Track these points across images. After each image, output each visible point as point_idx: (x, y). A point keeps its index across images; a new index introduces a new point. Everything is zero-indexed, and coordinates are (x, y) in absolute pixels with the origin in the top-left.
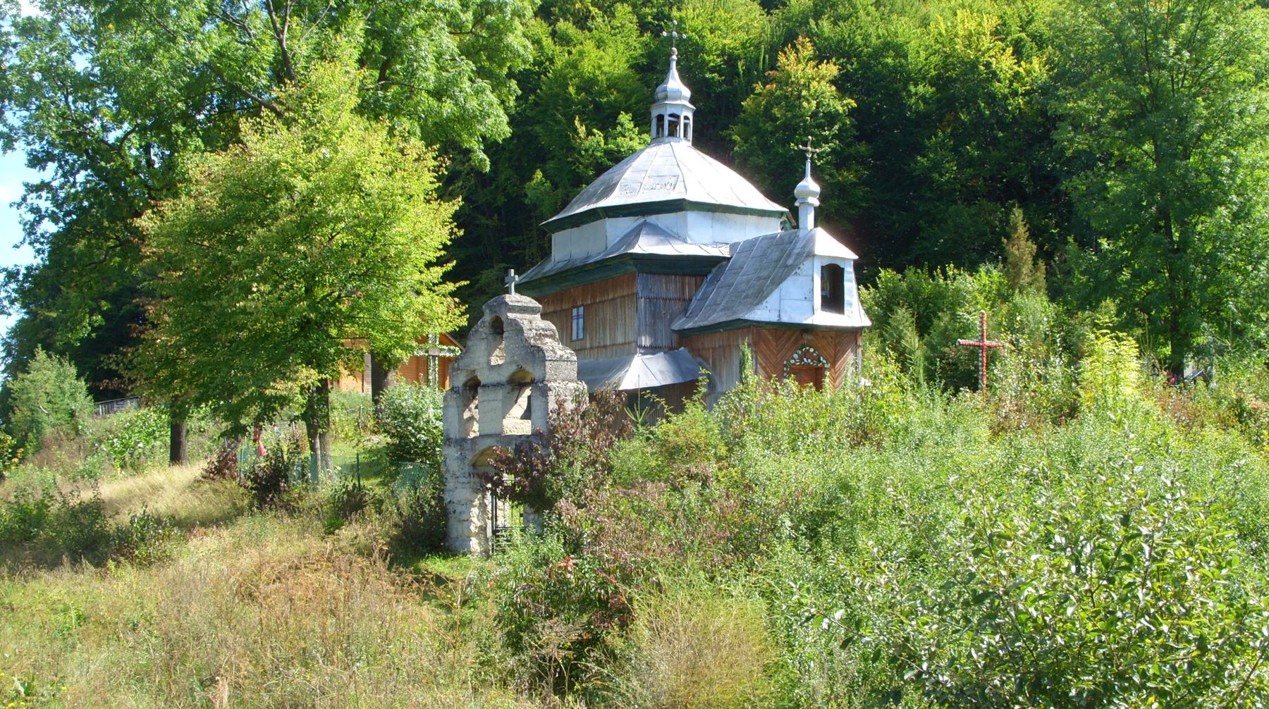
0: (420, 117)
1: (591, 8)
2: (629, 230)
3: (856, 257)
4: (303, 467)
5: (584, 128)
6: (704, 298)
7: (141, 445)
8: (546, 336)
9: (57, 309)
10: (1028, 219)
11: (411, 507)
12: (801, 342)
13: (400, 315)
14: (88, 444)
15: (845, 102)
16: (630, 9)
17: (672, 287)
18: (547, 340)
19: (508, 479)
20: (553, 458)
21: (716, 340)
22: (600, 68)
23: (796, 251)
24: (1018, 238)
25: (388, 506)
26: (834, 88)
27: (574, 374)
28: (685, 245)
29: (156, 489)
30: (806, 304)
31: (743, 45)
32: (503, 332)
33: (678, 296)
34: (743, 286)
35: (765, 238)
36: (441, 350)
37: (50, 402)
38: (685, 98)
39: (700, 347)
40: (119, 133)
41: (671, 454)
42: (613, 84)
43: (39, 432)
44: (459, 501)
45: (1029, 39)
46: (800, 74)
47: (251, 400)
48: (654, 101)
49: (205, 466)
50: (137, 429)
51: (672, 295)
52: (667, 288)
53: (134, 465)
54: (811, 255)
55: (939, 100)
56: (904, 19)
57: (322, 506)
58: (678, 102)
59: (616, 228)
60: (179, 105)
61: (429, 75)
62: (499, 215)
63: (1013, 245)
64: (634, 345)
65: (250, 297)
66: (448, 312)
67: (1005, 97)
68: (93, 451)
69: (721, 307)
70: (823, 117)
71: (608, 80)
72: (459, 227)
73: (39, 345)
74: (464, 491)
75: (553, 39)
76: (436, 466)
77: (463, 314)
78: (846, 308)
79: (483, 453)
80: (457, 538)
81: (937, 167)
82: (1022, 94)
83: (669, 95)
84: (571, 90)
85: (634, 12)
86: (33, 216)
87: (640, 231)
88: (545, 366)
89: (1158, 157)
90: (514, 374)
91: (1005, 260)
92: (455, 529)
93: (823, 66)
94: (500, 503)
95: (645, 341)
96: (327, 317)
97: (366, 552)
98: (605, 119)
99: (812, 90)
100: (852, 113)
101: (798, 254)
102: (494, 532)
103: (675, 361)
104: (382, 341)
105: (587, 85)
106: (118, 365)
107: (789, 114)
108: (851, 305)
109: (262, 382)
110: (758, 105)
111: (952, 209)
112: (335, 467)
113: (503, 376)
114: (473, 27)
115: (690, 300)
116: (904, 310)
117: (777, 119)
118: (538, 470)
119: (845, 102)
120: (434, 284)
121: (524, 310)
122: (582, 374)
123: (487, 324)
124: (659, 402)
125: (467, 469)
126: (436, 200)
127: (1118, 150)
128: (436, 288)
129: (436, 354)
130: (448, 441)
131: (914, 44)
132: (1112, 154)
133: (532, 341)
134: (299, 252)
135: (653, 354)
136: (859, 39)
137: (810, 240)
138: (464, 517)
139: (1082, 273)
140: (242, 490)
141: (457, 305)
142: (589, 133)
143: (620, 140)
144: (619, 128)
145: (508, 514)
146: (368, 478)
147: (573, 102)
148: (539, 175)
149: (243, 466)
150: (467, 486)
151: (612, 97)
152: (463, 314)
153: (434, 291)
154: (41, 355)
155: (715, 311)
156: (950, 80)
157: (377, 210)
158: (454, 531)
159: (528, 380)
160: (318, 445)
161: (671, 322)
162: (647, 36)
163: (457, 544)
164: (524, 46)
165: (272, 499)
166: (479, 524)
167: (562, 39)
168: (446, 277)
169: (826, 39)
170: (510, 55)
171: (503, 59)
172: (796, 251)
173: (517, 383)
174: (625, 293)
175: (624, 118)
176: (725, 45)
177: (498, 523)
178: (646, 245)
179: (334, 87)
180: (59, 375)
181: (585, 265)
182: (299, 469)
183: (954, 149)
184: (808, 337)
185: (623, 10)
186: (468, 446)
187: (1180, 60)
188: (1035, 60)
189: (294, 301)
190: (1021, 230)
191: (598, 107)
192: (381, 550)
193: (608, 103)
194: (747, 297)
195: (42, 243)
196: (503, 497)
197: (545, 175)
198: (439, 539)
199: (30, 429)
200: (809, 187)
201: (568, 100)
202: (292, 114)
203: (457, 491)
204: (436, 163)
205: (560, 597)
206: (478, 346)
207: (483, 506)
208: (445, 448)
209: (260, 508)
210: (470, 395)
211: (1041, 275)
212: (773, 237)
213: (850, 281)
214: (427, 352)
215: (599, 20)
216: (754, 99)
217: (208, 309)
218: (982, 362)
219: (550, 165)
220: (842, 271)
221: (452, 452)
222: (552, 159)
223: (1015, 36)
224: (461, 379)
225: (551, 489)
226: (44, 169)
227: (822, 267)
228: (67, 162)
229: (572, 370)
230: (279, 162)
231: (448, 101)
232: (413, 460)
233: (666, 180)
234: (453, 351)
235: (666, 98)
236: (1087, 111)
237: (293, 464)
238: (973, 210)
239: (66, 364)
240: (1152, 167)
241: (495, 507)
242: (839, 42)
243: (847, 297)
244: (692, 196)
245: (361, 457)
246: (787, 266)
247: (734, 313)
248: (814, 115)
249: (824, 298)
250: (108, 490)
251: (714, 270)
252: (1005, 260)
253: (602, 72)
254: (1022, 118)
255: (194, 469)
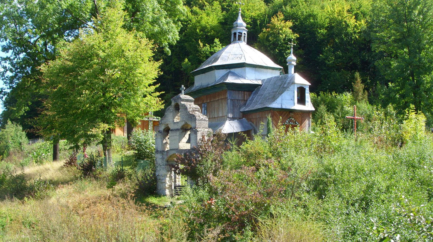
0: (146, 32)
1: (205, 3)
2: (224, 74)
3: (310, 84)
4: (101, 162)
5: (202, 44)
6: (252, 99)
7: (44, 154)
8: (196, 111)
9: (16, 107)
10: (360, 75)
11: (143, 178)
12: (289, 116)
13: (139, 103)
14: (25, 154)
15: (295, 35)
16: (219, 3)
17: (240, 96)
18: (197, 112)
19: (181, 166)
20: (200, 159)
21: (258, 115)
22: (208, 23)
23: (287, 82)
24: (358, 83)
25: (133, 176)
26: (291, 30)
27: (207, 126)
28: (245, 80)
29: (47, 170)
30: (292, 101)
31: (258, 16)
32: (179, 109)
33: (242, 99)
34: (267, 95)
35: (275, 77)
36: (154, 118)
37: (12, 139)
38: (244, 27)
39: (251, 117)
40: (35, 39)
41: (249, 156)
42: (213, 28)
43: (8, 150)
44: (162, 175)
45: (360, 13)
46: (279, 25)
47: (81, 136)
48: (232, 28)
49: (65, 161)
50: (42, 149)
51: (240, 99)
52: (239, 96)
53: (39, 162)
54: (293, 83)
55: (328, 35)
56: (316, 6)
57: (108, 177)
58: (242, 28)
59: (219, 74)
60: (56, 25)
61: (150, 16)
62: (172, 75)
63: (356, 85)
64: (226, 117)
65: (82, 96)
66: (157, 103)
67: (351, 34)
68: (27, 156)
69: (259, 103)
70: (287, 40)
71: (211, 27)
72: (161, 71)
73: (9, 119)
74: (164, 171)
75: (191, 13)
76: (153, 162)
77: (162, 104)
78: (306, 103)
79: (171, 156)
80: (161, 189)
81: (327, 58)
82: (357, 33)
83: (238, 25)
84: (198, 31)
85: (220, 4)
86: (4, 69)
87: (228, 74)
88: (196, 122)
89: (410, 53)
90: (184, 125)
91: (353, 91)
92: (160, 186)
93: (287, 23)
94: (177, 176)
95: (230, 115)
96: (111, 105)
97: (124, 196)
98: (210, 41)
99: (283, 31)
100: (297, 39)
101: (288, 83)
102: (175, 187)
103: (242, 124)
104: (131, 114)
105: (203, 29)
106: (31, 122)
107: (275, 39)
108: (308, 102)
109: (86, 129)
110: (264, 36)
111: (333, 73)
112: (113, 162)
113: (179, 126)
114: (165, 2)
115: (247, 100)
116: (323, 106)
117: (270, 41)
118: (194, 163)
119: (295, 35)
120: (152, 93)
121: (187, 101)
122: (210, 127)
123: (173, 106)
124: (244, 135)
125: (165, 163)
126: (153, 60)
127: (395, 51)
128: (152, 94)
129: (152, 120)
130: (157, 152)
131: (320, 14)
132: (393, 52)
133: (191, 113)
134: (100, 79)
135: (233, 120)
136: (300, 13)
137: (293, 78)
138: (163, 181)
139: (383, 95)
140: (78, 170)
141: (160, 101)
142: (204, 46)
143: (215, 48)
144: (215, 44)
145: (180, 180)
146: (126, 166)
147: (199, 35)
148: (186, 60)
149: (79, 162)
150: (165, 169)
151: (212, 33)
152: (162, 104)
153: (152, 95)
154: (9, 122)
155: (256, 104)
156: (333, 27)
157: (131, 64)
158: (159, 187)
159: (189, 128)
160: (107, 153)
161: (240, 108)
162: (224, 13)
163: (161, 191)
164: (184, 10)
165: (89, 174)
166: (169, 184)
167: (194, 13)
168: (157, 90)
169: (288, 13)
170: (178, 13)
171: (176, 14)
172: (287, 82)
173: (184, 129)
174: (223, 98)
175: (217, 40)
176: (252, 15)
177: (177, 183)
178: (230, 80)
179: (114, 18)
180: (16, 130)
181: (208, 87)
182: (100, 162)
183: (334, 52)
184: (292, 114)
185: (216, 3)
186: (165, 153)
187: (418, 18)
188: (362, 21)
189: (99, 98)
190: (359, 80)
191: (207, 36)
192: (131, 196)
193: (210, 35)
194: (269, 99)
195: (7, 80)
196: (179, 174)
197: (189, 60)
198: (154, 190)
199: (5, 149)
200: (292, 58)
201: (197, 34)
202: (99, 27)
203: (161, 171)
204: (152, 46)
205: (210, 216)
206: (169, 115)
207: (171, 177)
208: (156, 154)
209: (84, 177)
210: (165, 133)
211: (366, 96)
212: (278, 77)
213: (308, 93)
214: (148, 119)
215: (208, 7)
216: (262, 34)
217: (65, 101)
218: (355, 124)
219: (190, 56)
220: (305, 89)
221: (159, 156)
222: (192, 54)
223: (356, 12)
224: (162, 128)
225: (199, 170)
226: (8, 52)
227: (298, 88)
228: (16, 50)
229: (206, 124)
230: (93, 45)
231: (157, 26)
232: (143, 159)
233: (238, 56)
234: (158, 119)
235: (237, 26)
236: (384, 37)
237: (98, 161)
238: (340, 73)
239: (19, 126)
240: (407, 57)
241: (175, 178)
242: (293, 14)
243: (306, 99)
244: (248, 62)
245: (123, 159)
246: (284, 87)
247: (264, 105)
248: (284, 40)
249: (298, 99)
250: (28, 170)
251: (256, 89)
252: (353, 91)
253: (209, 24)
254: (357, 41)
255: (60, 163)
